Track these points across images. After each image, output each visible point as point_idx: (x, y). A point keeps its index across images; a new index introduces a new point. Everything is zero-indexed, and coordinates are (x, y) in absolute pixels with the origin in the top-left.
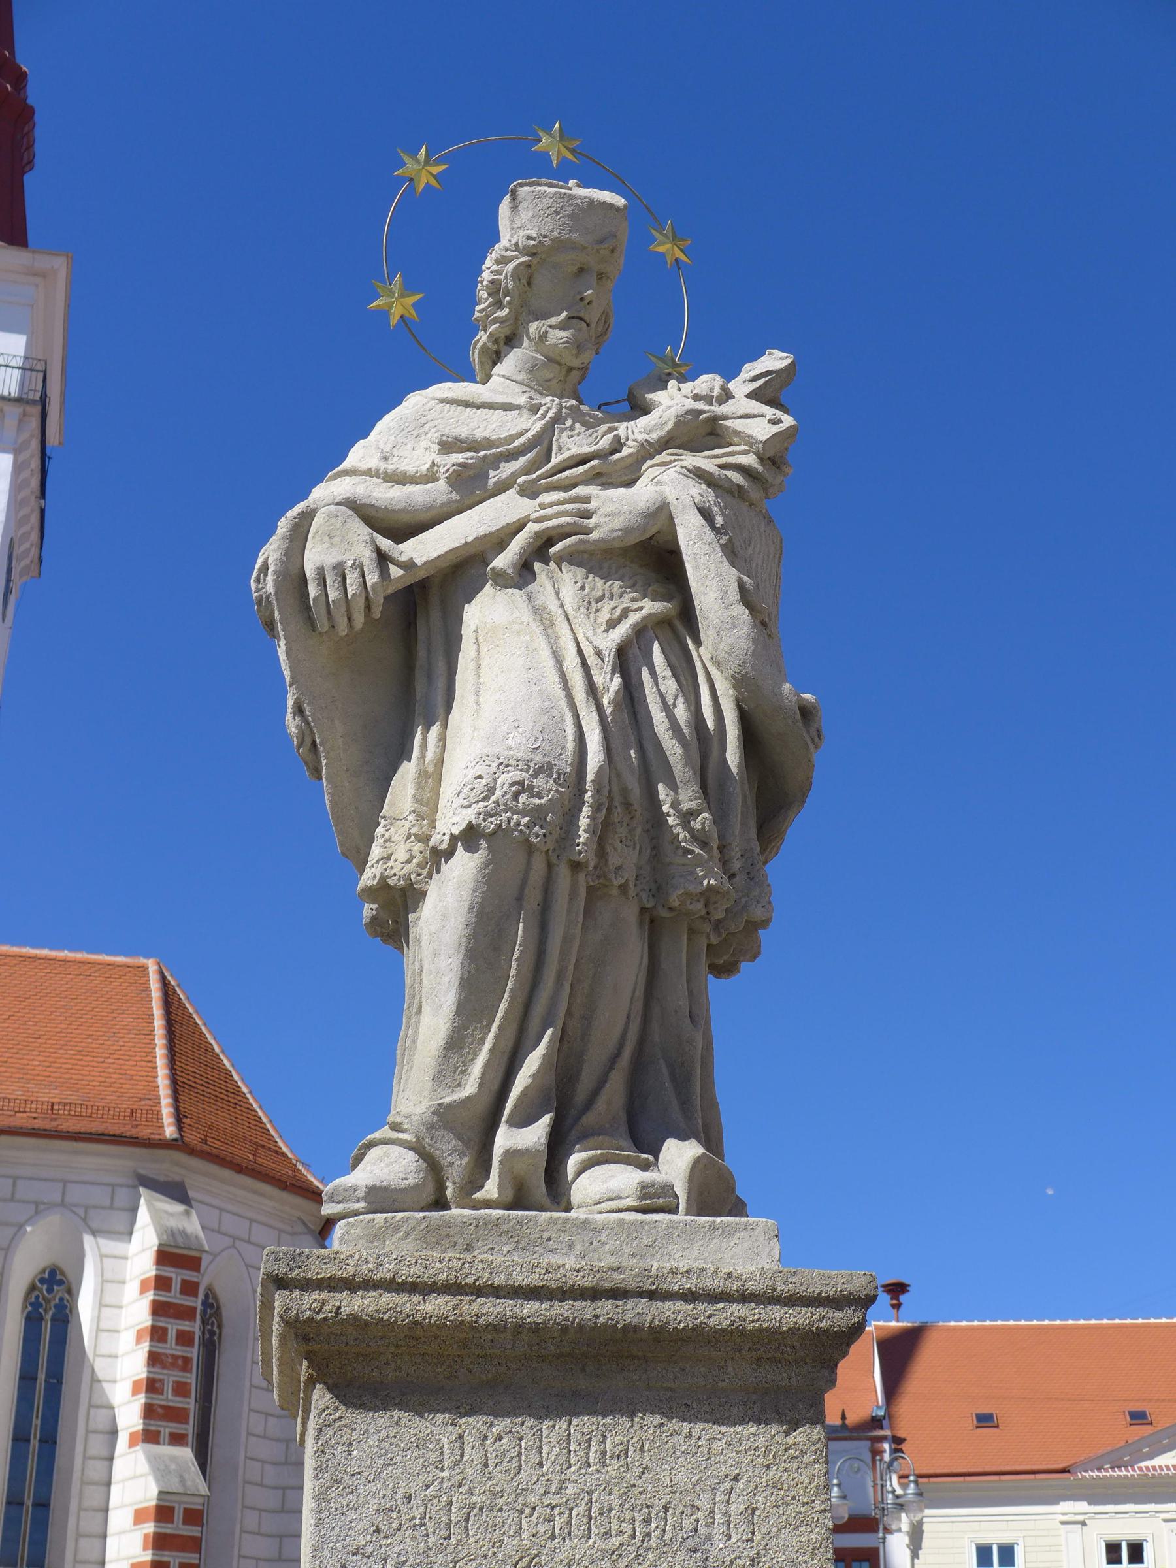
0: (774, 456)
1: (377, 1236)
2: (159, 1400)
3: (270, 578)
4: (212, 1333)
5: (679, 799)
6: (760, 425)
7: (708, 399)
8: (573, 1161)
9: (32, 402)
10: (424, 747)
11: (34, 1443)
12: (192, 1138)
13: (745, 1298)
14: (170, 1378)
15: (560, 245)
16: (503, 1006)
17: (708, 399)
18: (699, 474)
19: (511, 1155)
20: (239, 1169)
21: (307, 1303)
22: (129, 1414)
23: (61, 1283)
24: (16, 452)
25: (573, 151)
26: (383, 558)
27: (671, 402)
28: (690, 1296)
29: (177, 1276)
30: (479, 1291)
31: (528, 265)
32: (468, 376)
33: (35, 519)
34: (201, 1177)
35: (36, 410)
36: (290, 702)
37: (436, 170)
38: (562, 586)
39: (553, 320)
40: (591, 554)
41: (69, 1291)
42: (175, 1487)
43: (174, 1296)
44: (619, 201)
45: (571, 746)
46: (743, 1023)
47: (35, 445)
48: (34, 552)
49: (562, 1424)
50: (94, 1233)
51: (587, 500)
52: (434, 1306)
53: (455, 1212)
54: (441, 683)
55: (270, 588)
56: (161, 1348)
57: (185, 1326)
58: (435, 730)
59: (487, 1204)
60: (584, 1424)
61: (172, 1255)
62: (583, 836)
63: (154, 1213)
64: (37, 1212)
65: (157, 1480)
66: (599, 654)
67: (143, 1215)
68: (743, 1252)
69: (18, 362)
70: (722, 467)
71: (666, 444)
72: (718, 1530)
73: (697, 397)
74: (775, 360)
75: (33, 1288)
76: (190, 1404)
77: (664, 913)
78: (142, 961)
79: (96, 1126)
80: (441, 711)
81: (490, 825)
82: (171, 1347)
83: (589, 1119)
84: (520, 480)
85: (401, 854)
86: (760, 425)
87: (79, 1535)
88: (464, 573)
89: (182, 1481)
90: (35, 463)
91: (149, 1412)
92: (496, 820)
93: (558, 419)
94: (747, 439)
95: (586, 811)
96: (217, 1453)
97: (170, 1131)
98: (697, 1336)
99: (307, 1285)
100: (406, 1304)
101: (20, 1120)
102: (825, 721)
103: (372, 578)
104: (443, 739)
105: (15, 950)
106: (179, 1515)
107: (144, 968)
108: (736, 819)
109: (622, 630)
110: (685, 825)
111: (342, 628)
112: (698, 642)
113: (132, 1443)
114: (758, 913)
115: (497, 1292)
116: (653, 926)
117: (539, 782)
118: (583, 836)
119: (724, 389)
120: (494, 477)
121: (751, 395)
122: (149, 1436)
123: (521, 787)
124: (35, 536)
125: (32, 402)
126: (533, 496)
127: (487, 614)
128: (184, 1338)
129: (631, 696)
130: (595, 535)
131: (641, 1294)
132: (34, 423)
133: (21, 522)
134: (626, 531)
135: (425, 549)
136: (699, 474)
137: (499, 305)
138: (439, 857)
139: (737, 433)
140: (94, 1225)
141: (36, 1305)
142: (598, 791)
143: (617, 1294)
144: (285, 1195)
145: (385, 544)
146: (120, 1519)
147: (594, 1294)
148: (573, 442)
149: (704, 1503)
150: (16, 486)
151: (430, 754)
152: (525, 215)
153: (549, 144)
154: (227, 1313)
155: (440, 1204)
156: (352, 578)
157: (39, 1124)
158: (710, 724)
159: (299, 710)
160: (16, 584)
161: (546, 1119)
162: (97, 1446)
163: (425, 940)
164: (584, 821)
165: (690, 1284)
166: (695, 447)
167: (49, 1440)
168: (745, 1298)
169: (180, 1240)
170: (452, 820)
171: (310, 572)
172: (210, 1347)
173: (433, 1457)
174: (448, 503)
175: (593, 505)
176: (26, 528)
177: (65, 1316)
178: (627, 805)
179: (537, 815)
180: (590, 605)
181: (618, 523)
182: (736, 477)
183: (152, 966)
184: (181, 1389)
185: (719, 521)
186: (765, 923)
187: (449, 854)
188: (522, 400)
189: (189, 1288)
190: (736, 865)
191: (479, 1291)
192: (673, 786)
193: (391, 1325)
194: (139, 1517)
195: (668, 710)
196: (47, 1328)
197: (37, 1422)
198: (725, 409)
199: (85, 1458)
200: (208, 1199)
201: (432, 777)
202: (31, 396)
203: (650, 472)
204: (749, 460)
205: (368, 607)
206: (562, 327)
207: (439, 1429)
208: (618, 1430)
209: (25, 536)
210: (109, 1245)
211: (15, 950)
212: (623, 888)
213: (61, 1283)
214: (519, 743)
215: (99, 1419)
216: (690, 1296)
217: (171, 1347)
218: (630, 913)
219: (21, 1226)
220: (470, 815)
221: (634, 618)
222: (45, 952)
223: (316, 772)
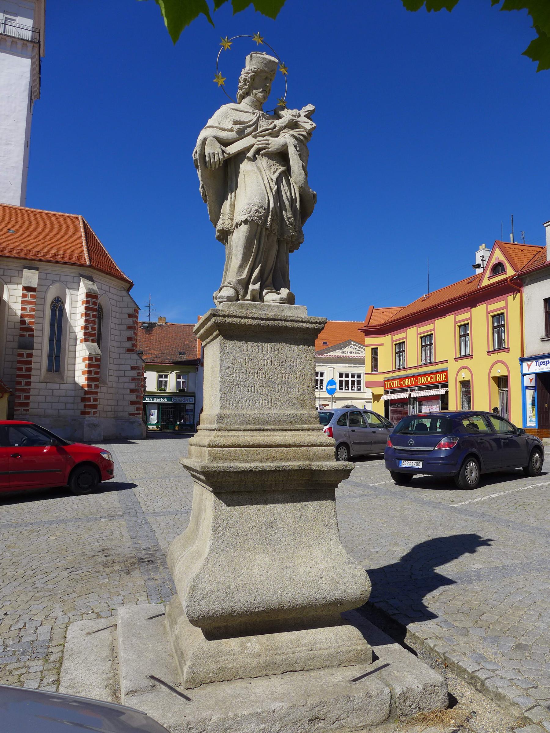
0: (310, 133)
1: (230, 306)
3: (197, 155)
4: (100, 315)
5: (287, 215)
6: (308, 125)
7: (295, 116)
8: (265, 292)
9: (35, 43)
10: (231, 198)
11: (55, 341)
12: (94, 265)
13: (302, 322)
14: (91, 326)
15: (262, 71)
16: (251, 259)
17: (295, 116)
18: (293, 136)
19: (253, 290)
20: (107, 273)
21: (219, 319)
22: (80, 335)
23: (60, 301)
24: (32, 59)
25: (262, 41)
26: (223, 152)
27: (287, 115)
28: (292, 321)
29: (91, 300)
30: (252, 318)
31: (254, 75)
32: (235, 101)
33: (38, 80)
34: (96, 275)
35: (37, 45)
36: (201, 185)
37: (230, 44)
38: (263, 162)
39: (259, 90)
40: (269, 154)
41: (63, 303)
43: (91, 305)
44: (277, 61)
45: (267, 202)
46: (296, 261)
47: (37, 56)
48: (38, 91)
49: (266, 344)
50: (69, 289)
51: (268, 140)
52: (244, 321)
53: (241, 302)
54: (234, 183)
55: (198, 157)
56: (88, 318)
57: (94, 313)
58: (233, 194)
59: (247, 300)
60: (271, 344)
62: (269, 223)
63: (85, 285)
64: (53, 283)
65: (88, 351)
66: (272, 180)
67: (82, 284)
68: (299, 313)
69: (31, 29)
70: (298, 134)
71: (285, 127)
72: (295, 365)
73: (293, 115)
74: (310, 107)
75: (53, 302)
76: (96, 332)
77: (282, 239)
78: (77, 216)
79: (68, 261)
80: (235, 189)
81: (250, 219)
82: (91, 318)
83: (267, 283)
84: (253, 133)
85: (227, 223)
86: (308, 125)
87: (68, 364)
88: (240, 156)
89: (95, 351)
90: (37, 63)
91: (85, 334)
92: (252, 218)
93: (259, 117)
94: (305, 128)
95: (270, 217)
96: (103, 345)
97: (88, 263)
98: (294, 328)
99: (219, 316)
100: (238, 320)
101: (47, 258)
102: (318, 198)
103: (221, 157)
104: (235, 196)
105: (41, 211)
106: (94, 359)
107: (78, 218)
108: (298, 220)
109: (277, 174)
110: (288, 220)
111: (213, 168)
112: (291, 177)
113: (81, 341)
114: (301, 241)
115: (256, 319)
116: (279, 242)
117: (260, 210)
118: (269, 223)
119: (299, 114)
120: (247, 132)
121: (305, 116)
122: (86, 340)
123: (257, 211)
124: (38, 86)
125: (35, 43)
126: (256, 138)
127: (245, 167)
128: (94, 316)
129: (279, 191)
130: (270, 150)
131: (283, 320)
132: (37, 50)
134: (277, 149)
135: (232, 149)
136: (293, 136)
137: (245, 84)
138: (238, 225)
139: (302, 126)
140: (69, 287)
141: (54, 307)
142: (272, 212)
143: (279, 320)
144: (118, 280)
145: (223, 148)
146: (79, 360)
147: (274, 320)
148: (264, 124)
149: (292, 360)
150: (32, 70)
151: (232, 200)
152: (254, 62)
153: (257, 39)
155: (238, 300)
156: (216, 156)
157: (52, 259)
158: (294, 197)
159: (203, 187)
160: (34, 101)
161: (259, 283)
162: (72, 342)
163: (234, 243)
164: (269, 219)
165: (292, 318)
166: (292, 128)
167: (59, 341)
168: (302, 322)
169: (92, 291)
170: (240, 216)
171: (207, 154)
172: (100, 318)
173: (242, 350)
174: (237, 138)
175: (270, 142)
176: (36, 83)
178: (277, 215)
179: (260, 217)
180: (270, 167)
181: (275, 147)
182: (301, 137)
183: (80, 218)
184: (93, 329)
185: (298, 149)
186: (302, 243)
187: (240, 225)
188: (251, 111)
189: (95, 304)
190: (297, 229)
191: (252, 318)
192: (286, 212)
193: (236, 324)
194: (84, 360)
195: (286, 194)
196: (57, 313)
198: (299, 119)
199: (69, 345)
200: (98, 281)
201: (233, 205)
202: (35, 40)
203: (282, 134)
204: (304, 133)
205: (219, 164)
206: (261, 92)
207: (244, 344)
208: (277, 345)
209: (35, 85)
210: (73, 292)
211: (41, 211)
212: (275, 234)
213: (60, 301)
214: (256, 201)
215: (72, 336)
216: (292, 321)
217: (91, 318)
218: (275, 239)
219: (49, 286)
220: (246, 217)
221: (279, 171)
222: (50, 212)
223: (206, 202)
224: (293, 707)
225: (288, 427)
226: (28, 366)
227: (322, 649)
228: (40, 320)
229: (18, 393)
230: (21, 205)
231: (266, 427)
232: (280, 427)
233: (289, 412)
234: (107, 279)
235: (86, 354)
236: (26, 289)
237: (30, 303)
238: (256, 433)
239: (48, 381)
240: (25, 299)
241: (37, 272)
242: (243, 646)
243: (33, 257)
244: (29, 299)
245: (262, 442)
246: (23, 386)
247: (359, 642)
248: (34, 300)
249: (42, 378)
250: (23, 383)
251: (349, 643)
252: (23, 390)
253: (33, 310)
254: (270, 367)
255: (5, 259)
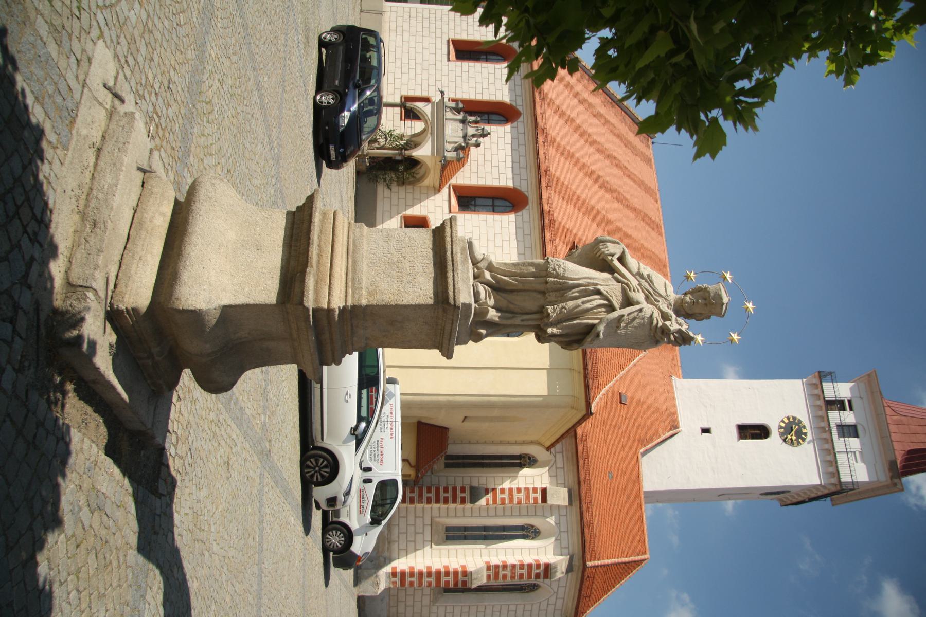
2: (500, 569)
11: (484, 533)
12: (588, 572)
14: (508, 572)
20: (580, 590)
22: (495, 561)
33: (800, 499)
34: (575, 576)
42: (474, 576)
57: (525, 576)
61: (548, 570)
63: (562, 560)
69: (855, 480)
75: (533, 526)
76: (500, 582)
82: (518, 572)
97: (589, 564)
106: (465, 579)
107: (645, 554)
124: (794, 501)
128: (521, 576)
133: (798, 495)
141: (527, 528)
154: (532, 594)
157: (585, 520)
177: (521, 466)
197: (491, 533)
217: (518, 572)
224: (112, 208)
225: (350, 277)
226: (450, 499)
227: (138, 267)
228: (508, 513)
229: (416, 490)
230: (645, 492)
231: (350, 260)
232: (350, 268)
233: (364, 278)
234: (573, 592)
235: (471, 568)
236: (544, 492)
237: (527, 497)
238: (345, 249)
239: (434, 527)
240: (531, 491)
241: (567, 503)
242: (163, 215)
243: (583, 498)
244: (532, 495)
245: (336, 247)
246: (425, 495)
247: (131, 300)
248: (532, 501)
249: (438, 520)
250: (429, 495)
251: (134, 292)
252: (421, 495)
253: (519, 503)
254: (407, 265)
255: (575, 467)
